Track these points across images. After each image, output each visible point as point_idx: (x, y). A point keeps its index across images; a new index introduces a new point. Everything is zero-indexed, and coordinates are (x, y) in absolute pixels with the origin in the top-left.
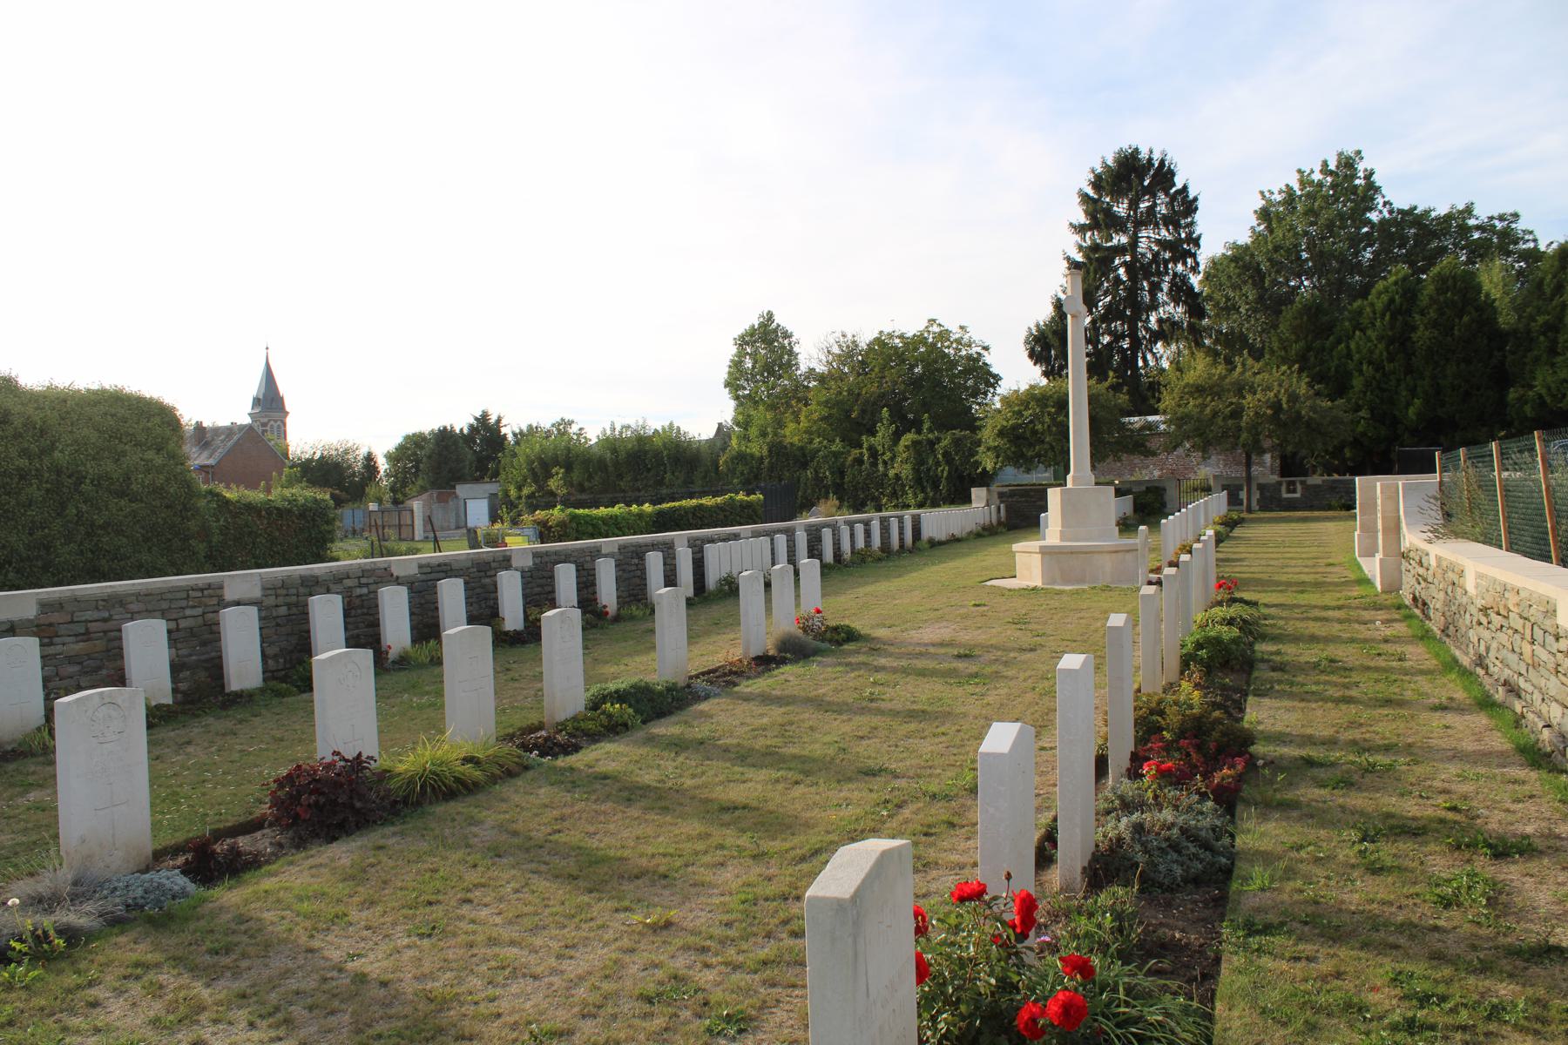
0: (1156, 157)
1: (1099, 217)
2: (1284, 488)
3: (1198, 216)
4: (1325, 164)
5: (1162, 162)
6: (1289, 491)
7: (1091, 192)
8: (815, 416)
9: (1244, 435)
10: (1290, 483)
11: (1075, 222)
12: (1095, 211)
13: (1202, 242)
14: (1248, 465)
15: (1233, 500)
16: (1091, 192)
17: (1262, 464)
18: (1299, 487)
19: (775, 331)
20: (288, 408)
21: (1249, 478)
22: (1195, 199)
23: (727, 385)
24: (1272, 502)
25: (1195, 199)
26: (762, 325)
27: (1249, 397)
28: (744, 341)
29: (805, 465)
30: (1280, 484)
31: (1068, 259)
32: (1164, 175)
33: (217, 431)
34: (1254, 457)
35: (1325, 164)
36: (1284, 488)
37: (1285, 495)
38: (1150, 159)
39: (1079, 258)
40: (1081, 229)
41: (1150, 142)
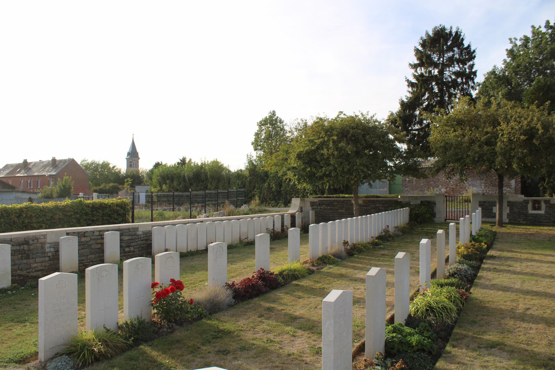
0: (454, 31)
1: (423, 59)
2: (530, 206)
3: (476, 61)
4: (548, 22)
5: (457, 33)
6: (534, 208)
7: (420, 48)
8: (281, 157)
9: (499, 159)
10: (535, 202)
11: (412, 63)
12: (422, 56)
13: (477, 74)
14: (501, 186)
15: (487, 213)
16: (420, 48)
17: (509, 186)
18: (543, 206)
19: (276, 120)
20: (139, 157)
21: (501, 197)
22: (474, 51)
23: (253, 144)
24: (519, 216)
25: (474, 51)
26: (270, 117)
27: (504, 126)
28: (263, 123)
29: (264, 181)
30: (527, 202)
31: (408, 81)
32: (457, 39)
33: (61, 161)
34: (506, 180)
35: (548, 22)
36: (530, 206)
37: (531, 212)
38: (451, 32)
39: (414, 81)
40: (415, 67)
41: (451, 24)
